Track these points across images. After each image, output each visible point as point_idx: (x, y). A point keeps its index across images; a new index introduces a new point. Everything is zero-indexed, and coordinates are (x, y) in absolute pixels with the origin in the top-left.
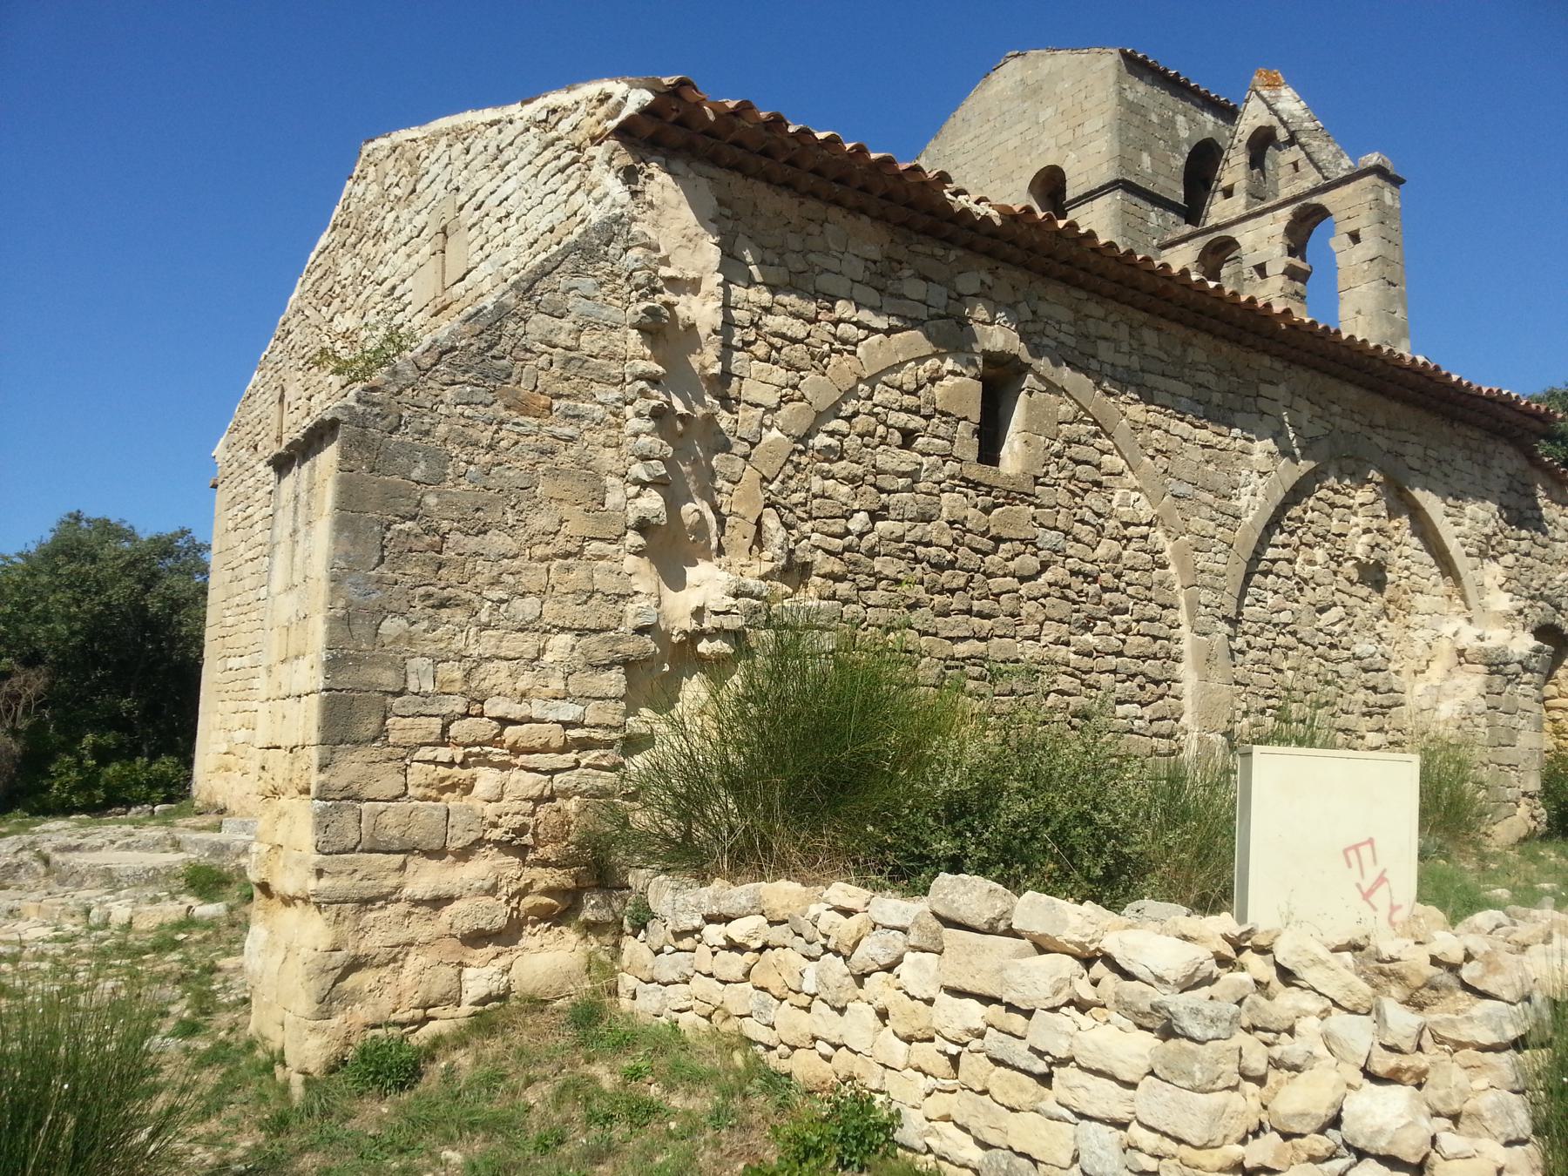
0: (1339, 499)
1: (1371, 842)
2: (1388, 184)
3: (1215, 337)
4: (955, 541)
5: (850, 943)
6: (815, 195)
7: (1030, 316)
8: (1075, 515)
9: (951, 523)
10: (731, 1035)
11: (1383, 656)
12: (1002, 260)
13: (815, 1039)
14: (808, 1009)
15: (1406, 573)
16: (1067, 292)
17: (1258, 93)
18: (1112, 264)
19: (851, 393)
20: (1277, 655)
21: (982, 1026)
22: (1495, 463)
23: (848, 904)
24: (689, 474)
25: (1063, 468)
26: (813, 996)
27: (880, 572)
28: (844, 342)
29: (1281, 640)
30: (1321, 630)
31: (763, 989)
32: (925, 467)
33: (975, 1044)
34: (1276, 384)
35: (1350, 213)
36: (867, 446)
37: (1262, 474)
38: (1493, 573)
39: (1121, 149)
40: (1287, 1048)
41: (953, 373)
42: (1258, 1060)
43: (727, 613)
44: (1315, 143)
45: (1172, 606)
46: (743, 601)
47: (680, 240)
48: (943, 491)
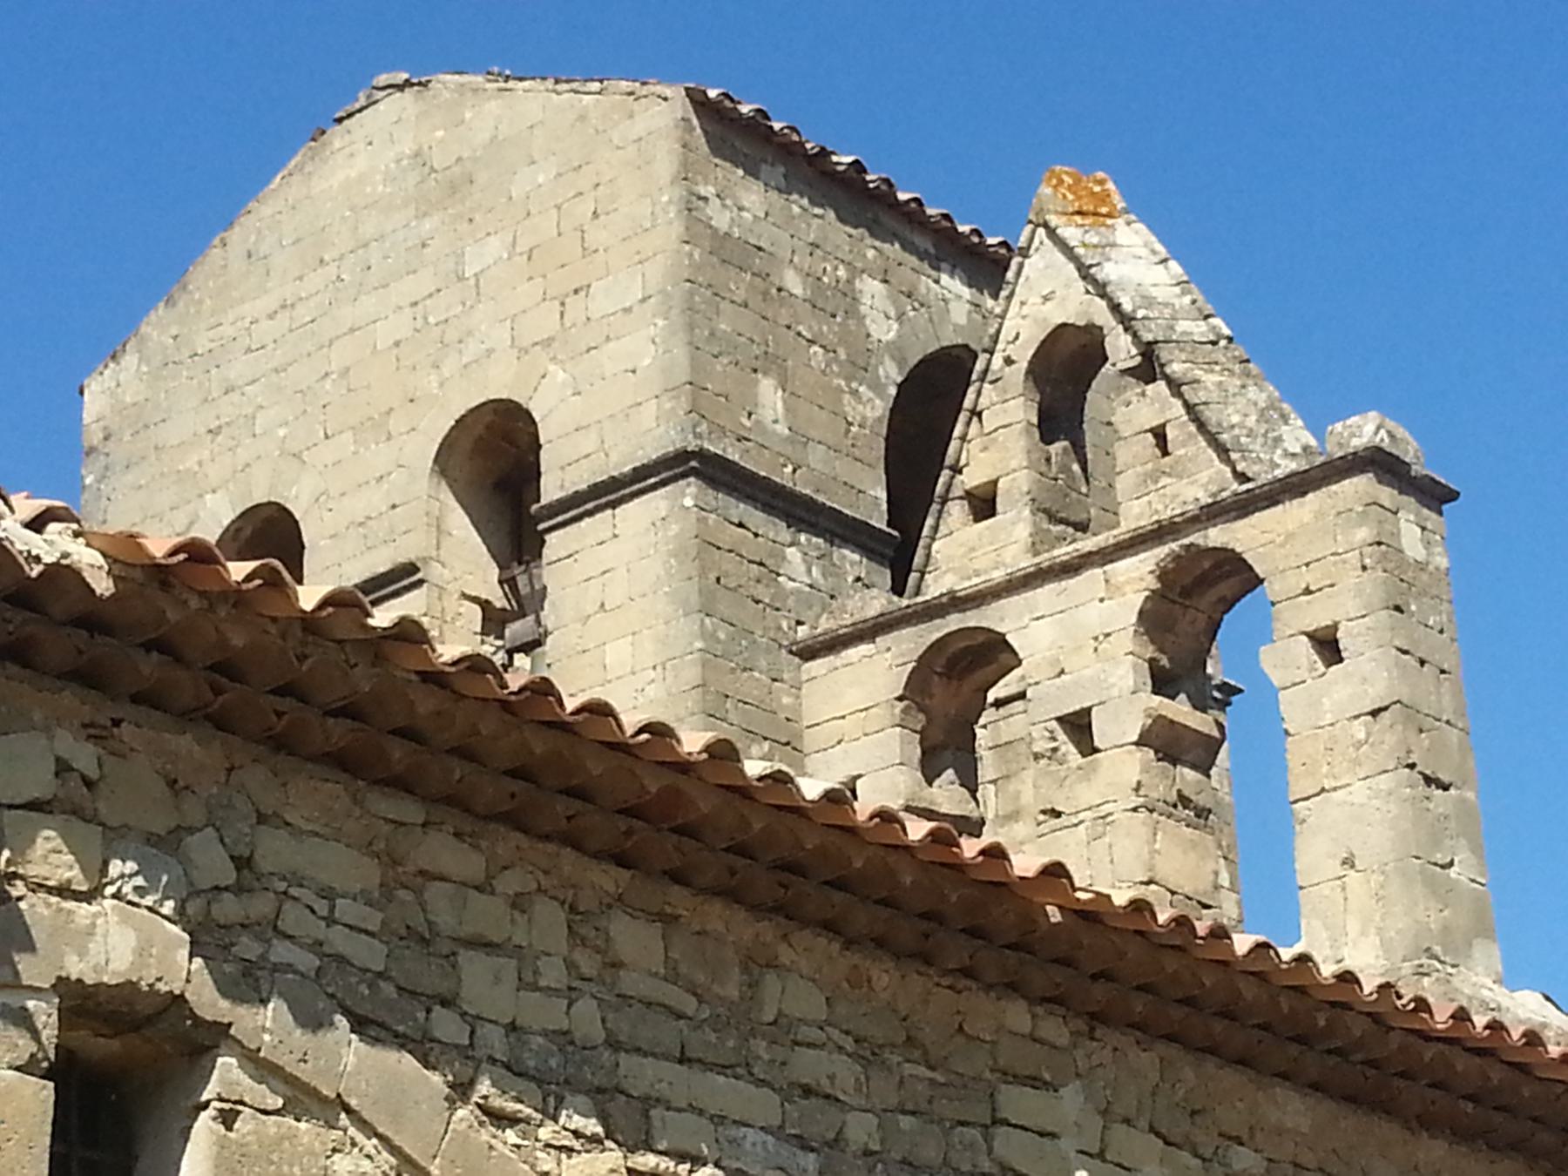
2: (1409, 501)
3: (849, 944)
7: (229, 876)
12: (136, 699)
17: (1052, 233)
18: (489, 724)
35: (1309, 578)
39: (695, 365)
44: (1210, 379)
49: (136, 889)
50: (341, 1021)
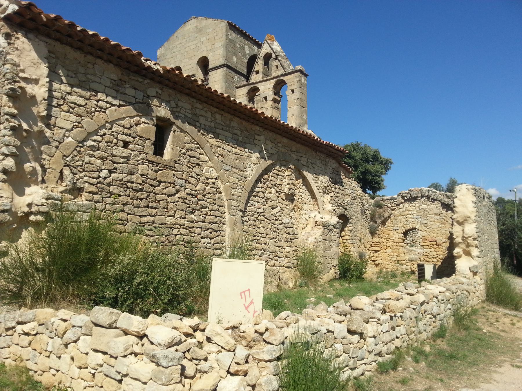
0: (280, 173)
1: (249, 290)
4: (143, 182)
5: (62, 333)
6: (91, 54)
7: (175, 106)
8: (189, 175)
9: (142, 175)
10: (22, 367)
11: (292, 223)
12: (165, 85)
13: (50, 368)
14: (48, 357)
15: (301, 197)
16: (189, 99)
17: (267, 42)
19: (103, 126)
20: (258, 223)
21: (102, 362)
22: (329, 165)
23: (65, 318)
24: (29, 152)
25: (186, 158)
26: (51, 352)
27: (112, 192)
28: (101, 108)
29: (259, 218)
30: (272, 215)
31: (35, 350)
32: (132, 155)
33: (100, 369)
34: (260, 136)
35: (292, 84)
36: (109, 146)
37: (255, 164)
38: (327, 198)
40: (203, 366)
41: (145, 123)
42: (191, 371)
43: (42, 205)
45: (222, 206)
46: (50, 201)
47: (30, 64)
48: (139, 164)
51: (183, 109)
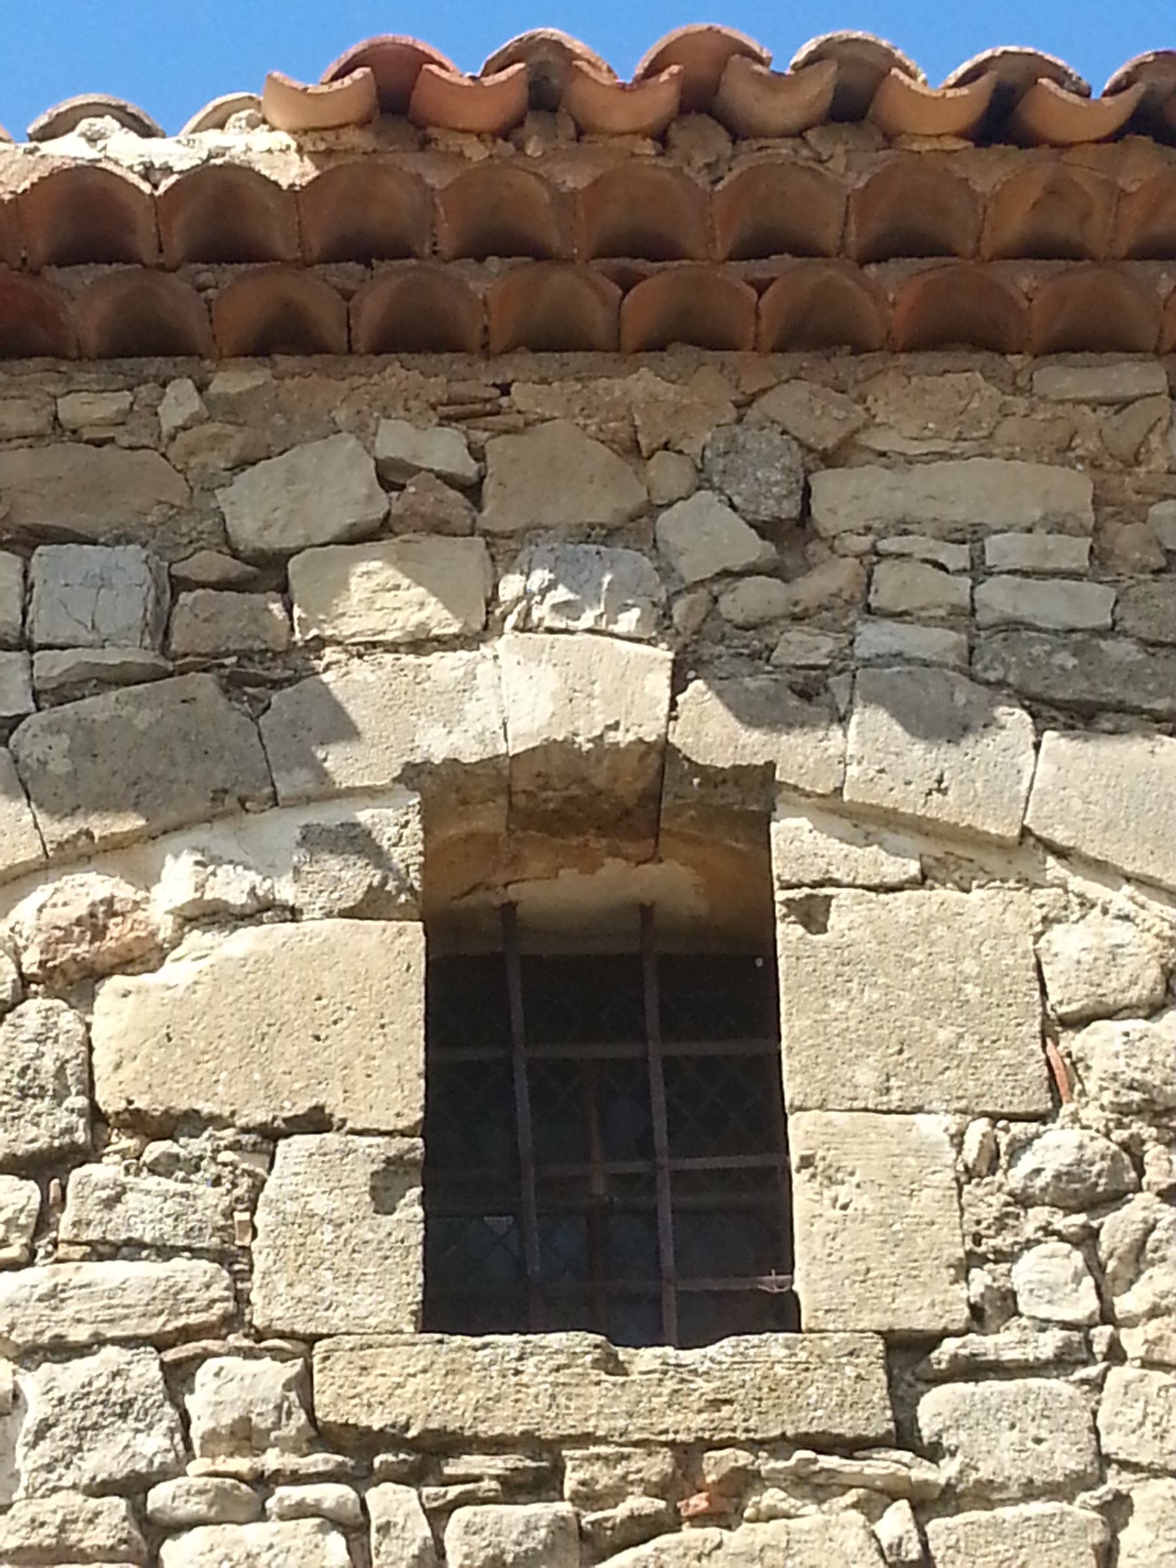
49: (557, 608)
50: (1015, 720)
51: (920, 545)
